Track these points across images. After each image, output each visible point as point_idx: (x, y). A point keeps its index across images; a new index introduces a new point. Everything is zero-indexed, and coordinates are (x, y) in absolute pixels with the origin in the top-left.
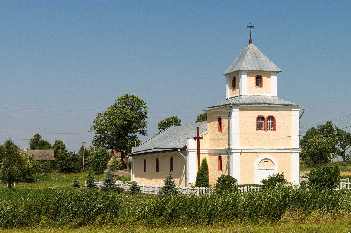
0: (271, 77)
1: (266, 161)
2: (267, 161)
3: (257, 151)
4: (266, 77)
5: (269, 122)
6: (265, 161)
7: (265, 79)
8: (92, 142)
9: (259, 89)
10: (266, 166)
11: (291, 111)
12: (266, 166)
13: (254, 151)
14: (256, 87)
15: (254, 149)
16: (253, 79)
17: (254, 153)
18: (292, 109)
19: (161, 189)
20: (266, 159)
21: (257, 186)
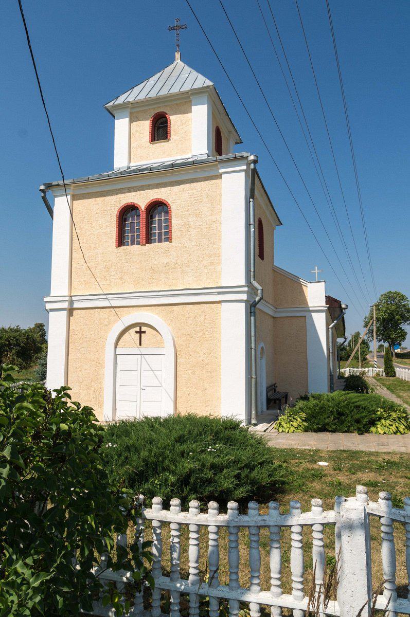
0: (189, 111)
1: (140, 329)
2: (143, 329)
3: (115, 303)
4: (181, 114)
5: (160, 220)
6: (138, 329)
7: (175, 120)
8: (61, 387)
9: (161, 146)
10: (140, 344)
11: (219, 177)
12: (140, 344)
13: (106, 304)
14: (153, 144)
15: (104, 297)
16: (144, 127)
17: (108, 310)
18: (221, 171)
19: (322, 549)
20: (140, 325)
21: (114, 409)
